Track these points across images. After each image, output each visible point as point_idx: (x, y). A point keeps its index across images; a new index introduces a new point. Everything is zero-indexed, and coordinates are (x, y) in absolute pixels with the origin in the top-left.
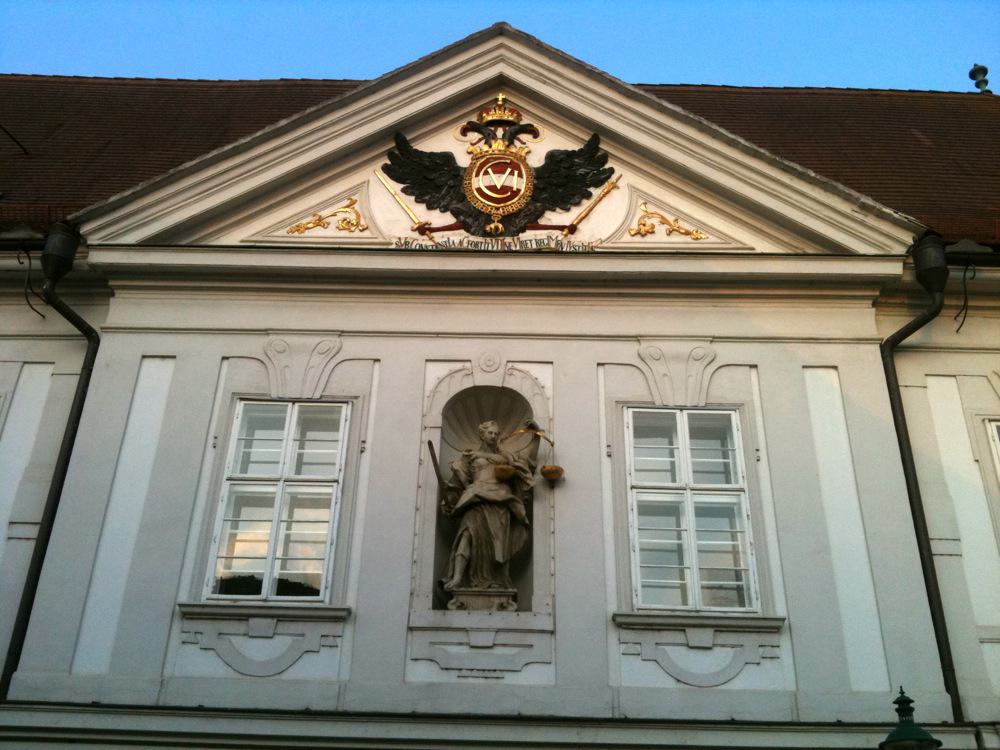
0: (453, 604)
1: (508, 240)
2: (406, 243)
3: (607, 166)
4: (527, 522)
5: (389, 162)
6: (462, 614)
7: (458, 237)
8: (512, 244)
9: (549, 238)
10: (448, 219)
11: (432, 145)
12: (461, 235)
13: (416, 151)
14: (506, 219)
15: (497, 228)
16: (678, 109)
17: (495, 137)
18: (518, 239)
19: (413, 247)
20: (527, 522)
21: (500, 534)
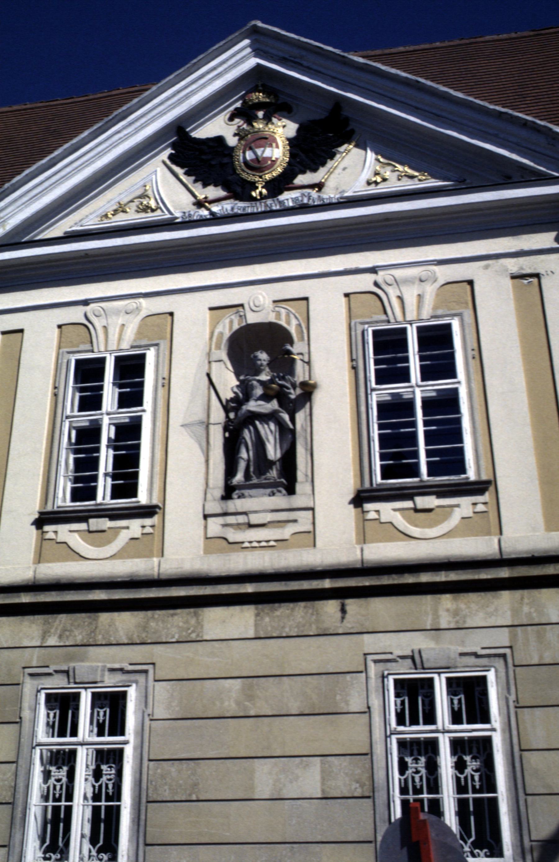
0: (237, 494)
1: (269, 202)
2: (190, 215)
3: (349, 129)
4: (291, 426)
5: (173, 152)
6: (242, 500)
7: (227, 207)
8: (273, 205)
9: (303, 195)
10: (219, 192)
11: (205, 131)
12: (231, 203)
13: (195, 138)
14: (268, 185)
15: (261, 193)
16: (86, 133)
17: (256, 118)
18: (278, 199)
19: (195, 218)
20: (291, 426)
21: (271, 439)
